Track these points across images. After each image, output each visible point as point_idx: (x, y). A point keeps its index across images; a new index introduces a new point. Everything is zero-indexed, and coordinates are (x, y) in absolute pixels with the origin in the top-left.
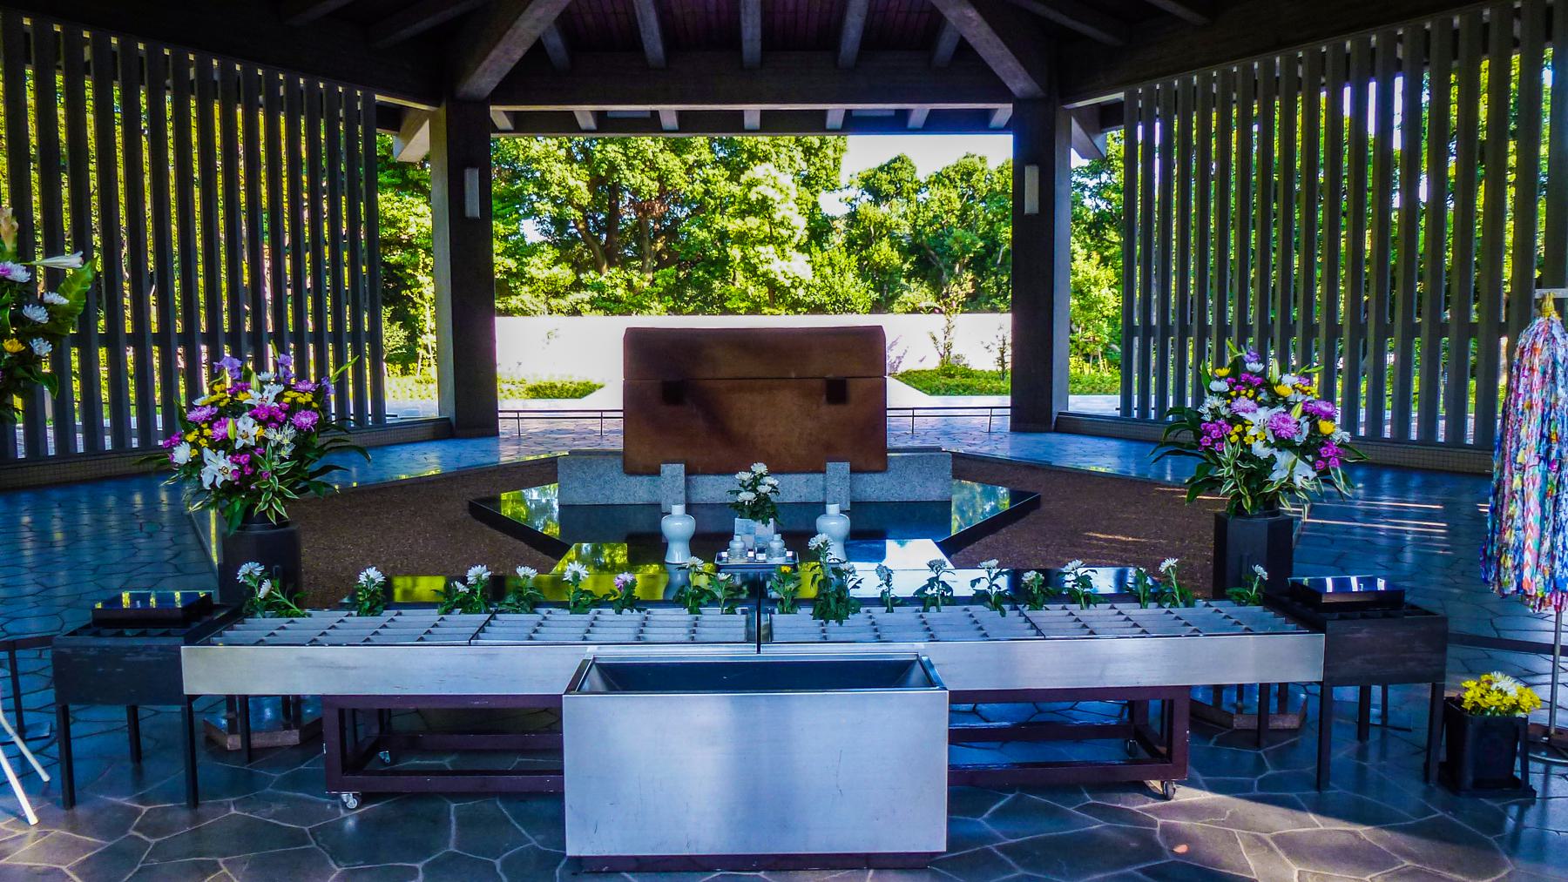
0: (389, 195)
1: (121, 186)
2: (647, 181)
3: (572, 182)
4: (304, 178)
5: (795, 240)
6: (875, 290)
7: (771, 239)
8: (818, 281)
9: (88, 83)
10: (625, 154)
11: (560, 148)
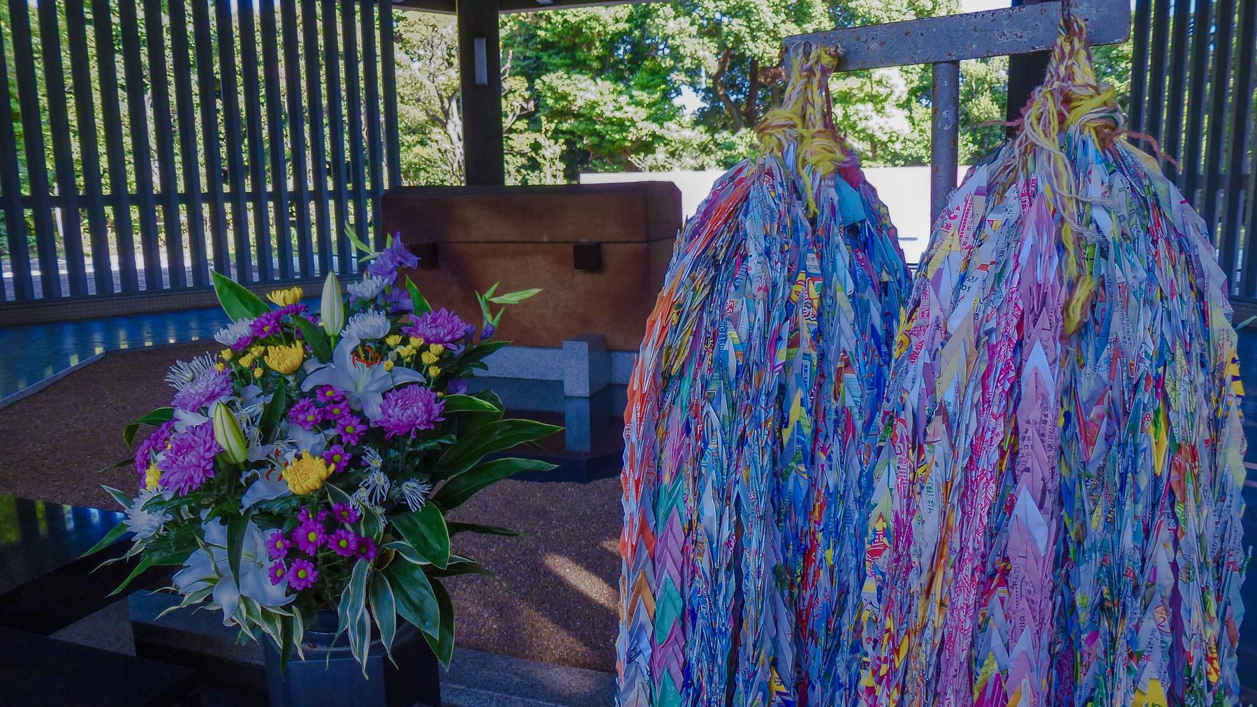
0: (560, 73)
1: (380, 81)
2: (768, 49)
3: (701, 54)
4: (1236, 17)
5: (894, 97)
6: (974, 142)
7: (872, 98)
8: (916, 135)
9: (376, 9)
10: (749, 27)
11: (692, 24)
